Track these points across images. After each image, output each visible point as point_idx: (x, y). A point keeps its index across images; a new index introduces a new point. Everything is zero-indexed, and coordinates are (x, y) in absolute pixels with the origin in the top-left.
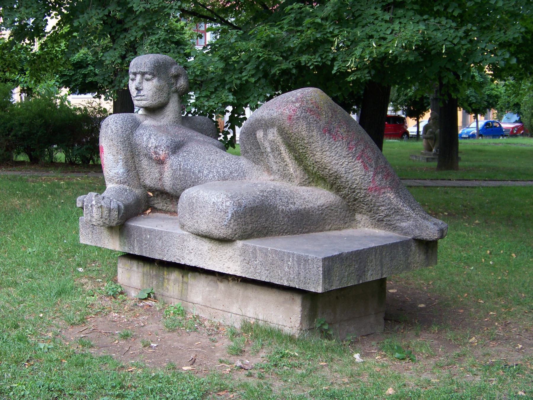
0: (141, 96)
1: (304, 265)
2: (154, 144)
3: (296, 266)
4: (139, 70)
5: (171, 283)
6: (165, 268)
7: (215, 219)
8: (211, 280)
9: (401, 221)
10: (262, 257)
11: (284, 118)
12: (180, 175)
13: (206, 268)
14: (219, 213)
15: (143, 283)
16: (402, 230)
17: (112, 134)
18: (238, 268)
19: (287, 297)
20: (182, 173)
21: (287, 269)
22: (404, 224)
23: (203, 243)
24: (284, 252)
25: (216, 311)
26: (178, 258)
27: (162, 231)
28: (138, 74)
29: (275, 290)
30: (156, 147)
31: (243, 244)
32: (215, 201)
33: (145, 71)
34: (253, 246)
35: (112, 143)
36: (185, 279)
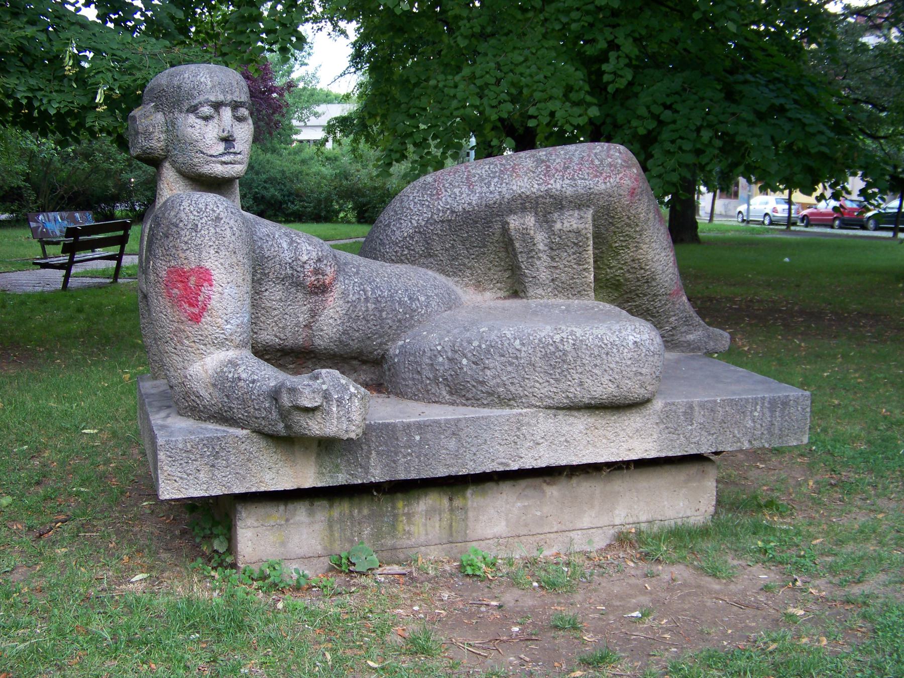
0: (235, 153)
1: (783, 410)
2: (314, 254)
3: (768, 414)
4: (229, 98)
5: (419, 520)
6: (399, 495)
7: (644, 371)
8: (527, 487)
9: (687, 334)
10: (704, 416)
11: (622, 193)
12: (367, 311)
13: (574, 463)
14: (651, 359)
15: (332, 540)
16: (690, 345)
17: (233, 238)
18: (649, 446)
19: (692, 472)
20: (371, 306)
21: (750, 424)
22: (691, 337)
23: (571, 419)
24: (747, 400)
25: (542, 537)
26: (504, 461)
27: (459, 420)
28: (226, 105)
29: (667, 468)
30: (319, 260)
31: (666, 404)
32: (638, 340)
33: (242, 100)
34: (687, 403)
35: (235, 260)
36: (458, 502)
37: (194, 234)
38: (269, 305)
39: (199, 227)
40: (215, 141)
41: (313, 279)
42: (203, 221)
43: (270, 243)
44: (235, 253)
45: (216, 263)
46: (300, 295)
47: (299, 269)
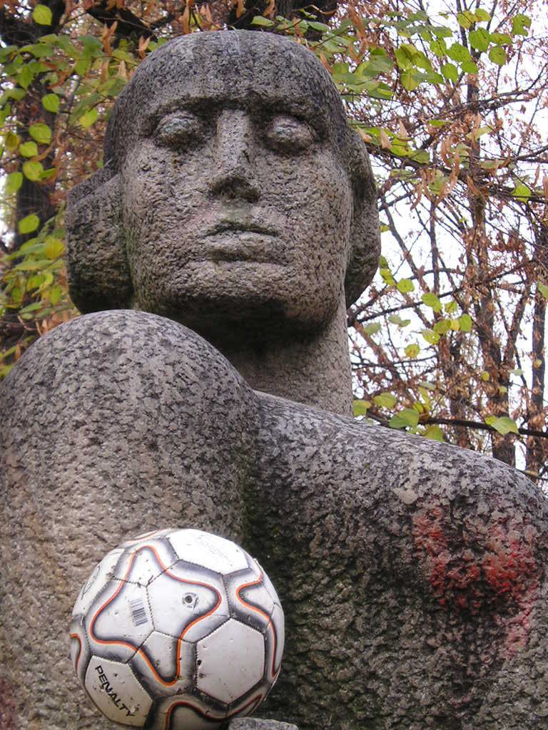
2: (445, 482)
17: (150, 404)
35: (150, 466)
37: (42, 397)
38: (321, 645)
39: (59, 375)
40: (200, 200)
41: (445, 558)
42: (72, 359)
43: (310, 450)
44: (153, 446)
45: (91, 472)
46: (412, 616)
47: (395, 526)
